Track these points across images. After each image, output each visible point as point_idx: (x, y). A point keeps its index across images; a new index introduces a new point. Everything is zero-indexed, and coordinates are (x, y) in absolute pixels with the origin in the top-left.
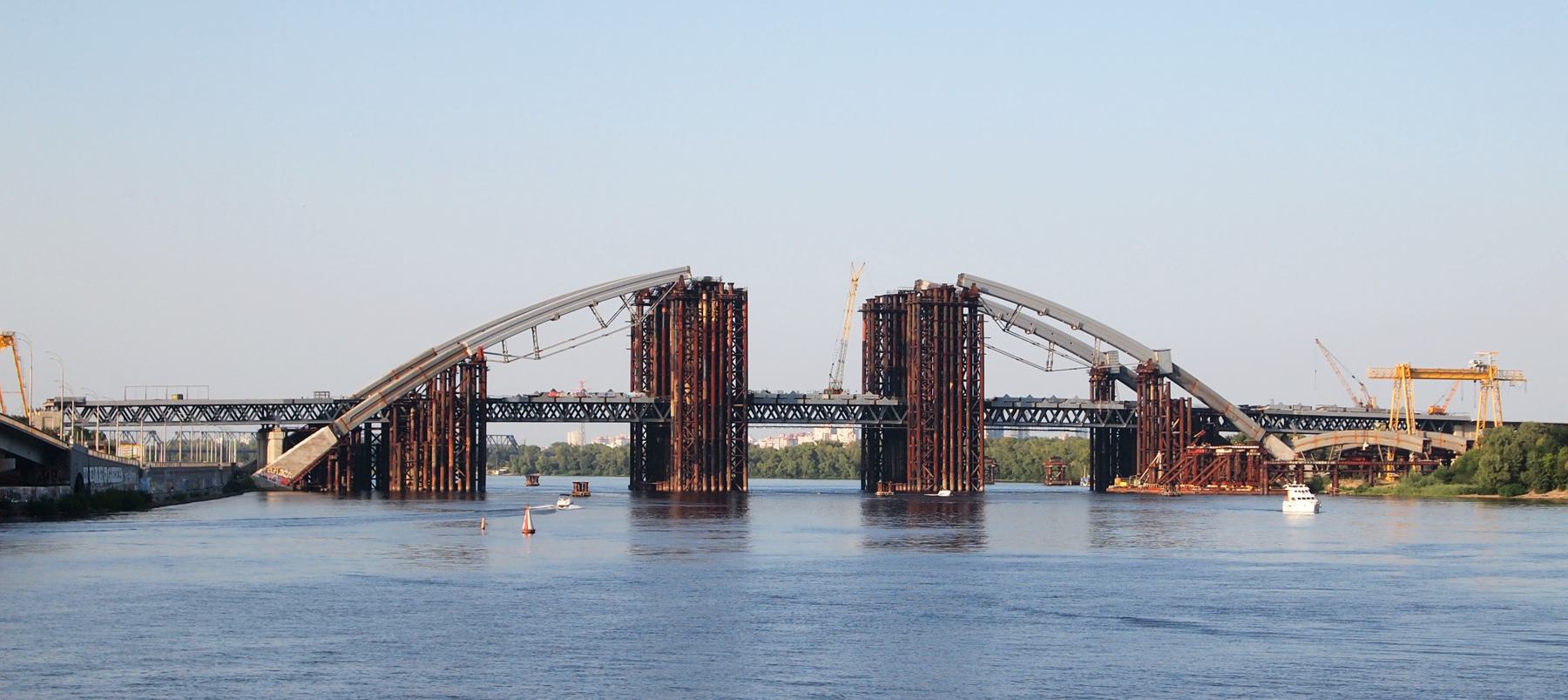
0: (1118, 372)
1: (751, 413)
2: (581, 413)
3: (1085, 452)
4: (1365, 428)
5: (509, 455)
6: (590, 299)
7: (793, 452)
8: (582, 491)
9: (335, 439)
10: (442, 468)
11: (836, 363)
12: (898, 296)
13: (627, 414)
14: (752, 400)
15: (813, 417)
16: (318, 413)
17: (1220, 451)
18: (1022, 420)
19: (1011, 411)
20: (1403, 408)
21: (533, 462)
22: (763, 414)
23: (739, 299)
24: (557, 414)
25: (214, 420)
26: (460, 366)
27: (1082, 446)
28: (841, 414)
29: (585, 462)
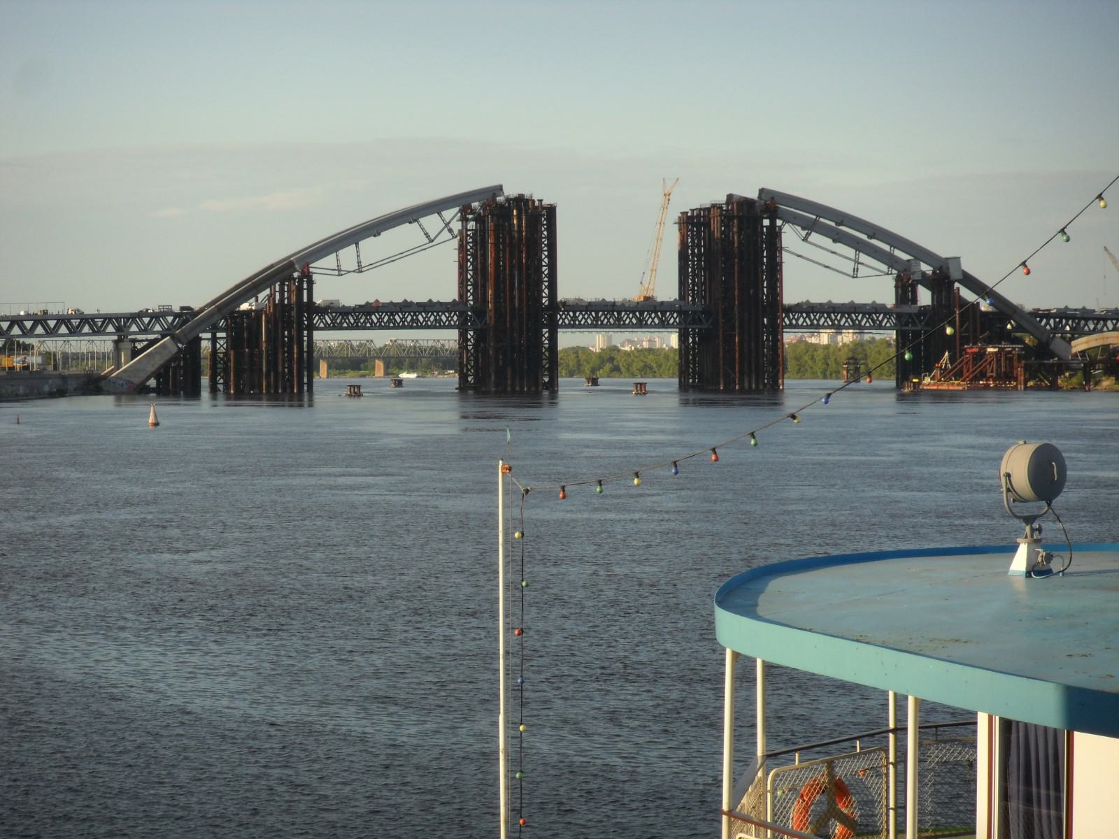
0: (920, 278)
1: (786, 320)
8: (641, 389)
9: (176, 348)
11: (648, 273)
13: (675, 321)
14: (312, 308)
22: (818, 321)
23: (551, 211)
29: (647, 363)
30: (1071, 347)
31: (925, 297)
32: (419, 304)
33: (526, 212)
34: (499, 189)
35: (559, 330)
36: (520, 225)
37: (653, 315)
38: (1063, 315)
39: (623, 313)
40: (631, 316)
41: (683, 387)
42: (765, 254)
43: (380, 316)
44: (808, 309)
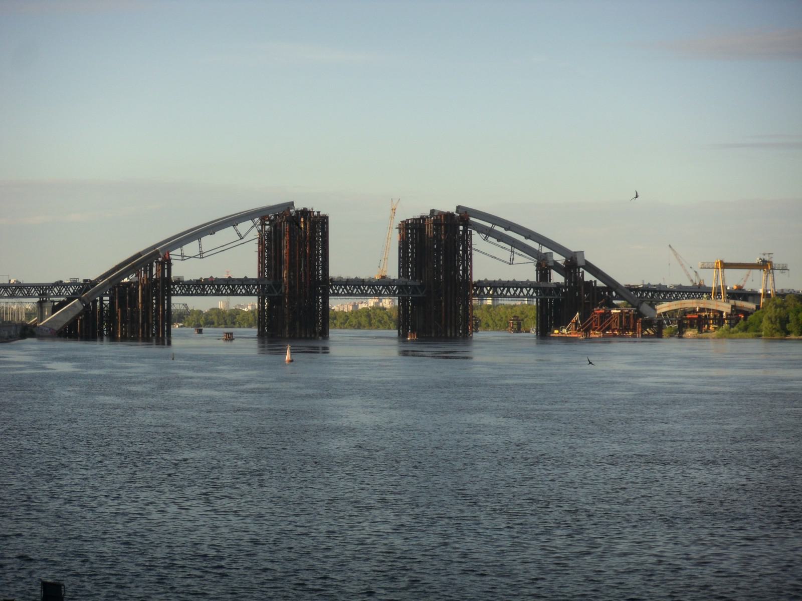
0: (553, 265)
1: (330, 290)
2: (213, 291)
3: (533, 313)
4: (697, 298)
5: (182, 317)
6: (233, 221)
7: (356, 312)
10: (145, 324)
12: (419, 219)
15: (368, 292)
16: (72, 291)
17: (614, 311)
18: (482, 294)
19: (502, 288)
20: (720, 286)
21: (198, 320)
22: (338, 291)
23: (323, 221)
24: (214, 291)
25: (12, 296)
26: (156, 262)
27: (532, 309)
28: (385, 291)
29: (231, 319)
30: (656, 310)
31: (557, 278)
32: (239, 280)
33: (310, 219)
34: (292, 204)
35: (330, 297)
36: (305, 228)
37: (241, 287)
38: (646, 289)
39: (206, 286)
40: (226, 288)
41: (261, 335)
42: (461, 249)
43: (60, 289)
44: (347, 283)
